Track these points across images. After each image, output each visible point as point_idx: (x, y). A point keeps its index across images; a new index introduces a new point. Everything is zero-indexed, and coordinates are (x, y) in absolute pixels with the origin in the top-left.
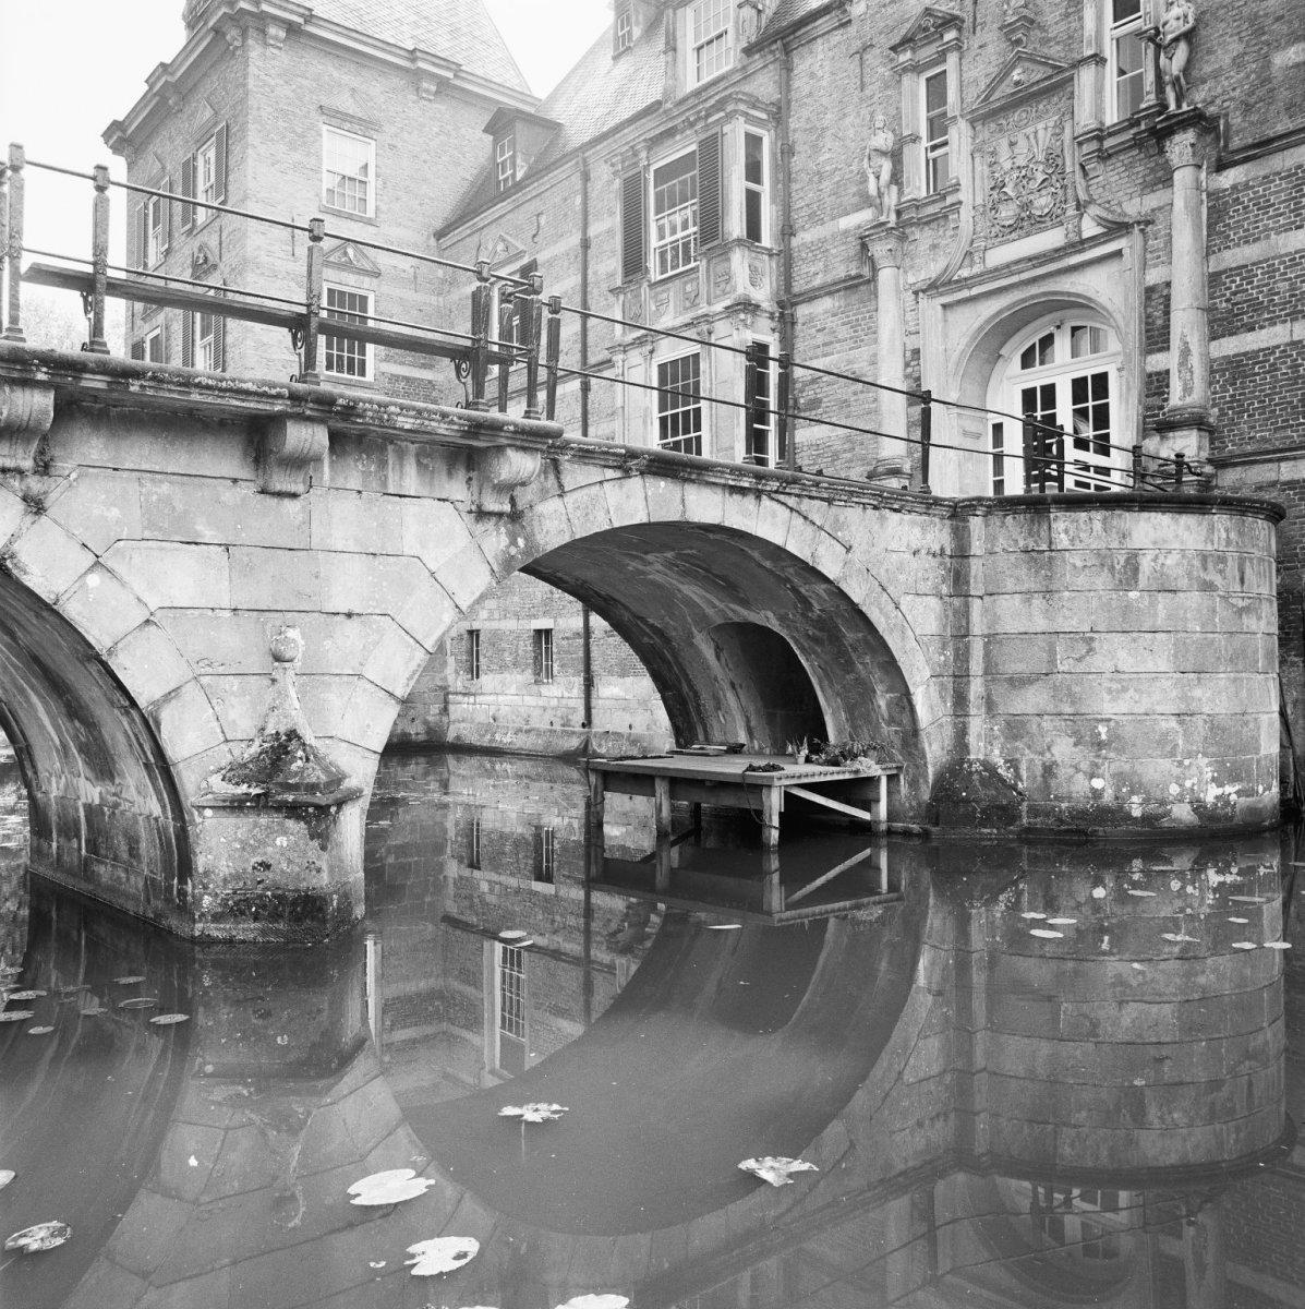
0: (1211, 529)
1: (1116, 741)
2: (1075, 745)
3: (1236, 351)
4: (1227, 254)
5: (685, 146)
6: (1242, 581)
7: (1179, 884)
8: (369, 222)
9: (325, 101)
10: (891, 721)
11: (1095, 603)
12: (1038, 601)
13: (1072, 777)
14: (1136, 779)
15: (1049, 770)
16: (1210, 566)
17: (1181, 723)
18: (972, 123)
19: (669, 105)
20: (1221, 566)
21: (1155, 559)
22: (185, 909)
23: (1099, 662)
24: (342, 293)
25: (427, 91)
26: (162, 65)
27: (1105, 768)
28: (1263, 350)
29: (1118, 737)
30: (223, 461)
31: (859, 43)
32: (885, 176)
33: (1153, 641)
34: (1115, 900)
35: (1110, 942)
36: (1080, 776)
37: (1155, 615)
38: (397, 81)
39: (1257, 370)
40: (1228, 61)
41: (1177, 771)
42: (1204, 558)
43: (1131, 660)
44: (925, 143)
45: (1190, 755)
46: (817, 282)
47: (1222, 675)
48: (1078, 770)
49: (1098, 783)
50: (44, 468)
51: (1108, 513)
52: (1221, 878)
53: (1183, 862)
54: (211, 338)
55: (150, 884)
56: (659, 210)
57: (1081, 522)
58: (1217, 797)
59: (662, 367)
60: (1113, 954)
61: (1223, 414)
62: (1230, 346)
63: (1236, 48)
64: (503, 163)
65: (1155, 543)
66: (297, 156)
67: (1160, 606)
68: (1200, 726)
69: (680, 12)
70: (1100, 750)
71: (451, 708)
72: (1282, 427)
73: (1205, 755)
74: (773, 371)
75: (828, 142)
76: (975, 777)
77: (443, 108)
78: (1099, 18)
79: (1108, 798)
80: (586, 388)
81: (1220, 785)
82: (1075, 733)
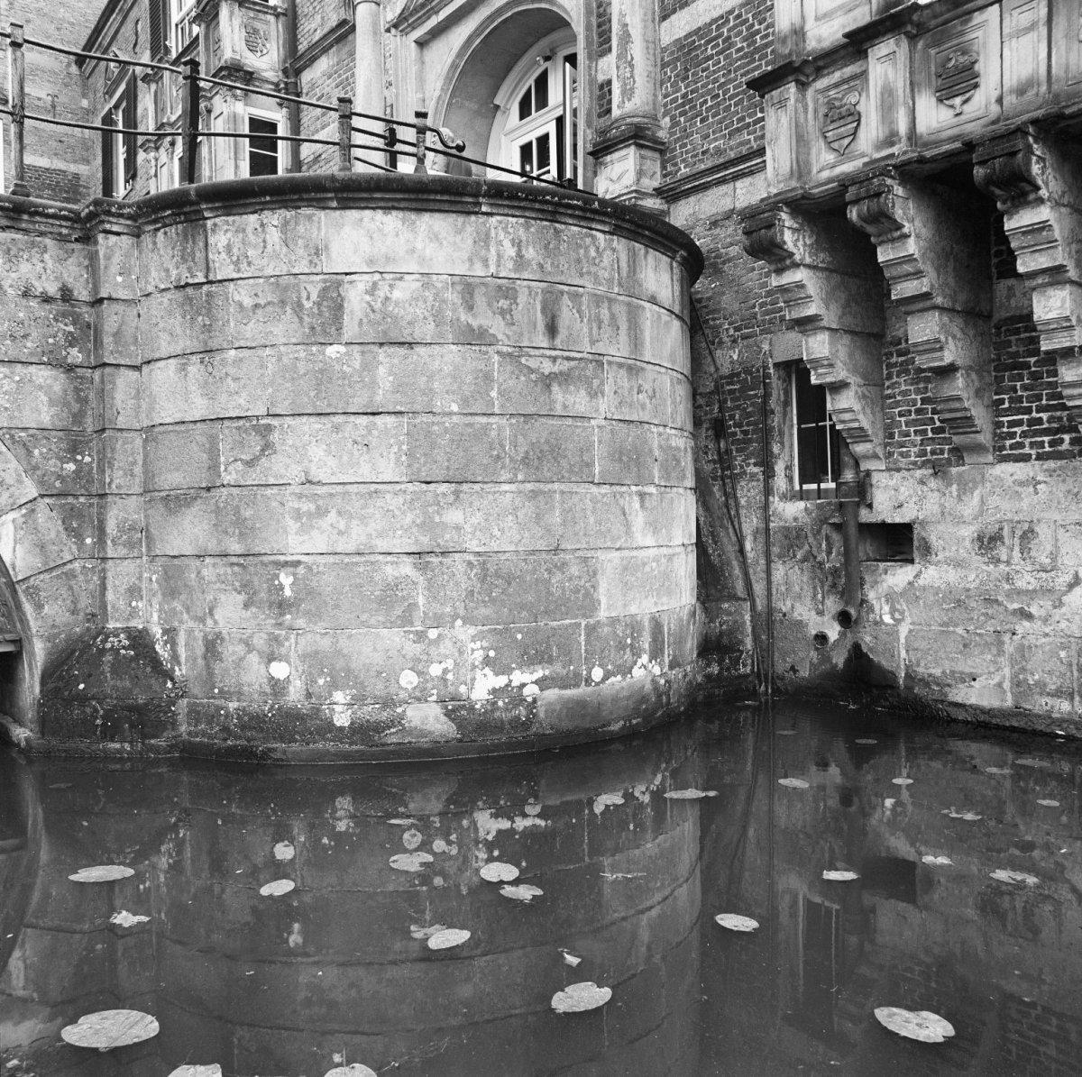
0: (484, 239)
2: (246, 606)
3: (688, 29)
6: (552, 330)
7: (419, 838)
11: (271, 367)
12: (195, 369)
13: (241, 659)
14: (340, 664)
15: (212, 647)
16: (480, 300)
17: (423, 568)
20: (504, 303)
21: (372, 290)
23: (282, 467)
27: (291, 644)
28: (715, 20)
29: (311, 592)
33: (369, 430)
34: (308, 862)
35: (303, 932)
36: (254, 658)
37: (373, 384)
39: (709, 52)
41: (413, 649)
42: (468, 288)
43: (332, 462)
47: (506, 487)
48: (249, 647)
49: (279, 670)
51: (289, 214)
52: (505, 824)
53: (431, 801)
57: (249, 230)
58: (494, 691)
60: (307, 955)
61: (675, 124)
65: (371, 262)
67: (382, 370)
70: (282, 614)
72: (738, 130)
73: (468, 621)
76: (108, 658)
79: (294, 695)
81: (501, 669)
82: (245, 586)
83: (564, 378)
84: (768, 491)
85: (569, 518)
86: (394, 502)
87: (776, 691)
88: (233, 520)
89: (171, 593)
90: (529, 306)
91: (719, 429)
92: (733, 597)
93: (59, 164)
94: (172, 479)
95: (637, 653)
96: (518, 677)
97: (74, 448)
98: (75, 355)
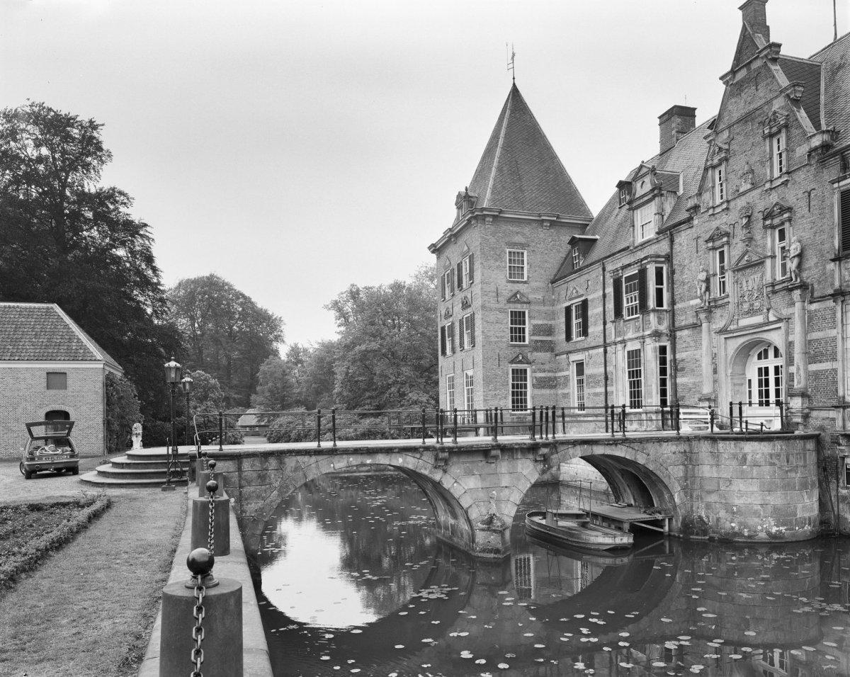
0: (775, 445)
1: (739, 512)
4: (814, 334)
5: (634, 271)
6: (788, 462)
8: (525, 282)
10: (670, 502)
15: (718, 520)
16: (773, 457)
17: (762, 507)
18: (734, 272)
19: (631, 248)
22: (474, 550)
23: (734, 488)
24: (516, 312)
31: (696, 235)
32: (703, 289)
38: (534, 225)
40: (813, 264)
41: (760, 522)
42: (771, 455)
44: (718, 276)
45: (766, 517)
46: (683, 324)
49: (733, 525)
54: (469, 331)
55: (466, 544)
56: (627, 293)
59: (629, 352)
62: (814, 367)
63: (815, 260)
64: (575, 257)
66: (498, 263)
68: (770, 508)
69: (635, 211)
71: (561, 468)
73: (771, 517)
74: (669, 357)
75: (686, 271)
78: (773, 241)
80: (605, 352)
83: (790, 471)
84: (838, 486)
85: (791, 498)
87: (840, 534)
90: (783, 458)
91: (825, 469)
92: (828, 511)
93: (546, 322)
95: (805, 525)
98: (686, 463)
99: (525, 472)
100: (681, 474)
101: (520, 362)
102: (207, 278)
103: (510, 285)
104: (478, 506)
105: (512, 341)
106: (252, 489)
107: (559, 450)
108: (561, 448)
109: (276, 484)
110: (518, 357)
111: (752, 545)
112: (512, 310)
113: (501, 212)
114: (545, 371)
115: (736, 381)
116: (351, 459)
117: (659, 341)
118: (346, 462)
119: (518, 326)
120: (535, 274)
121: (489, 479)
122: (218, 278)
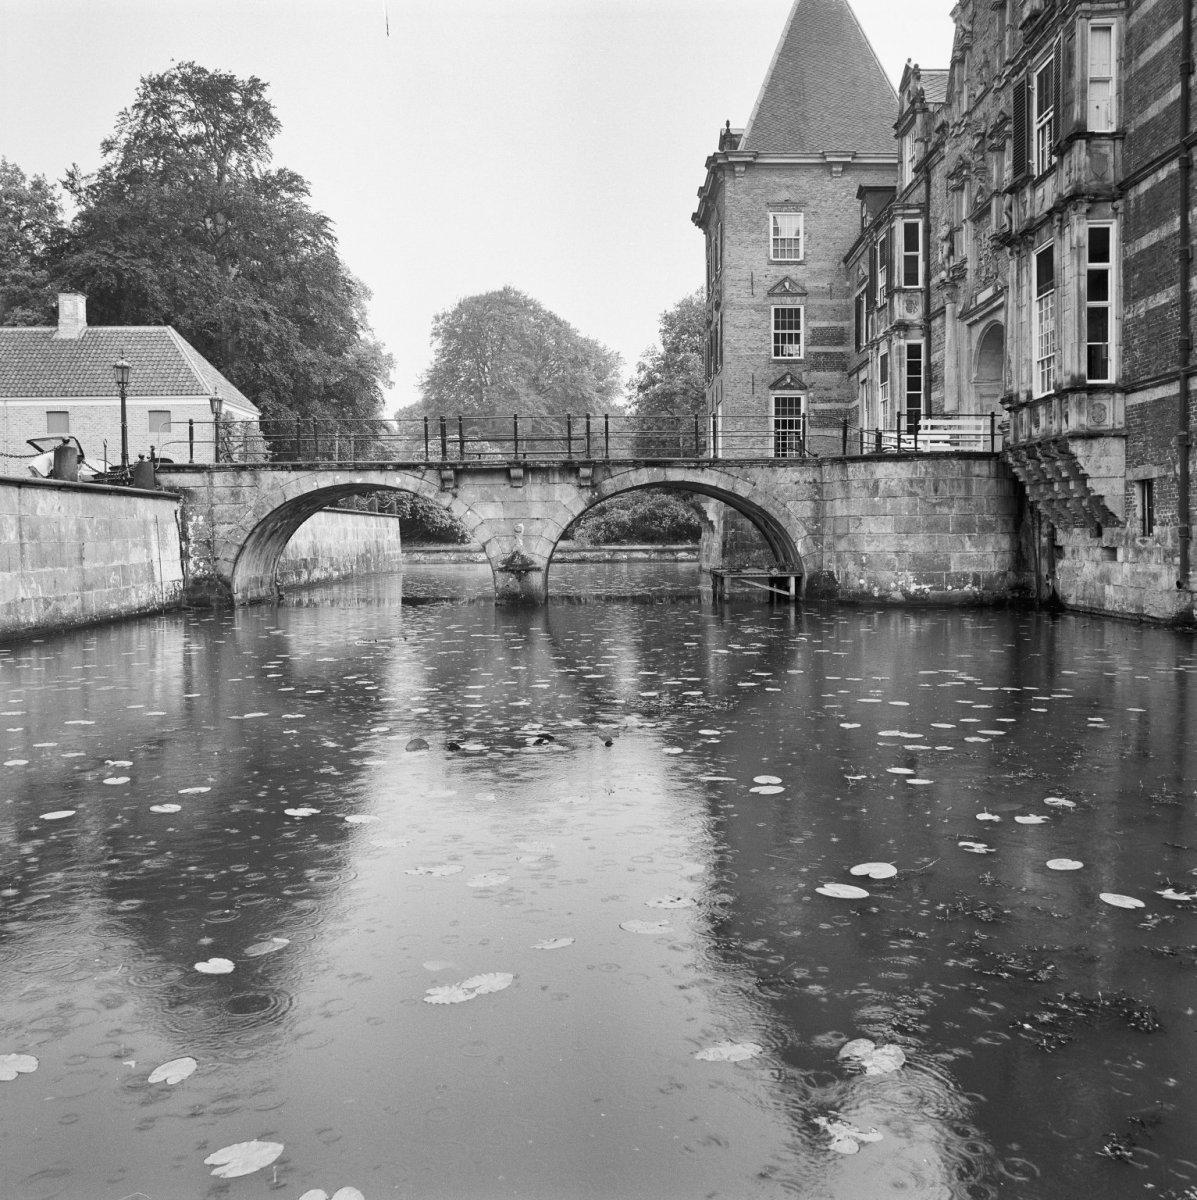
0: (916, 467)
6: (936, 491)
8: (799, 263)
9: (771, 199)
15: (847, 575)
17: (898, 556)
23: (864, 529)
24: (783, 310)
25: (837, 172)
26: (701, 188)
30: (500, 481)
38: (817, 171)
41: (894, 577)
42: (911, 482)
45: (901, 570)
49: (862, 581)
50: (456, 487)
66: (753, 236)
68: (907, 557)
77: (849, 178)
81: (918, 583)
83: (940, 504)
86: (891, 539)
88: (852, 542)
89: (838, 561)
90: (930, 485)
93: (834, 324)
94: (839, 531)
96: (923, 586)
97: (816, 522)
98: (817, 497)
99: (565, 501)
100: (808, 513)
101: (788, 387)
102: (500, 294)
103: (774, 269)
104: (498, 541)
105: (777, 354)
106: (225, 507)
107: (613, 473)
108: (616, 471)
109: (252, 504)
110: (783, 378)
111: (885, 605)
112: (778, 307)
113: (756, 155)
114: (829, 401)
115: (985, 391)
116: (338, 477)
117: (905, 337)
118: (331, 479)
119: (787, 331)
120: (818, 250)
121: (515, 507)
122: (516, 293)
